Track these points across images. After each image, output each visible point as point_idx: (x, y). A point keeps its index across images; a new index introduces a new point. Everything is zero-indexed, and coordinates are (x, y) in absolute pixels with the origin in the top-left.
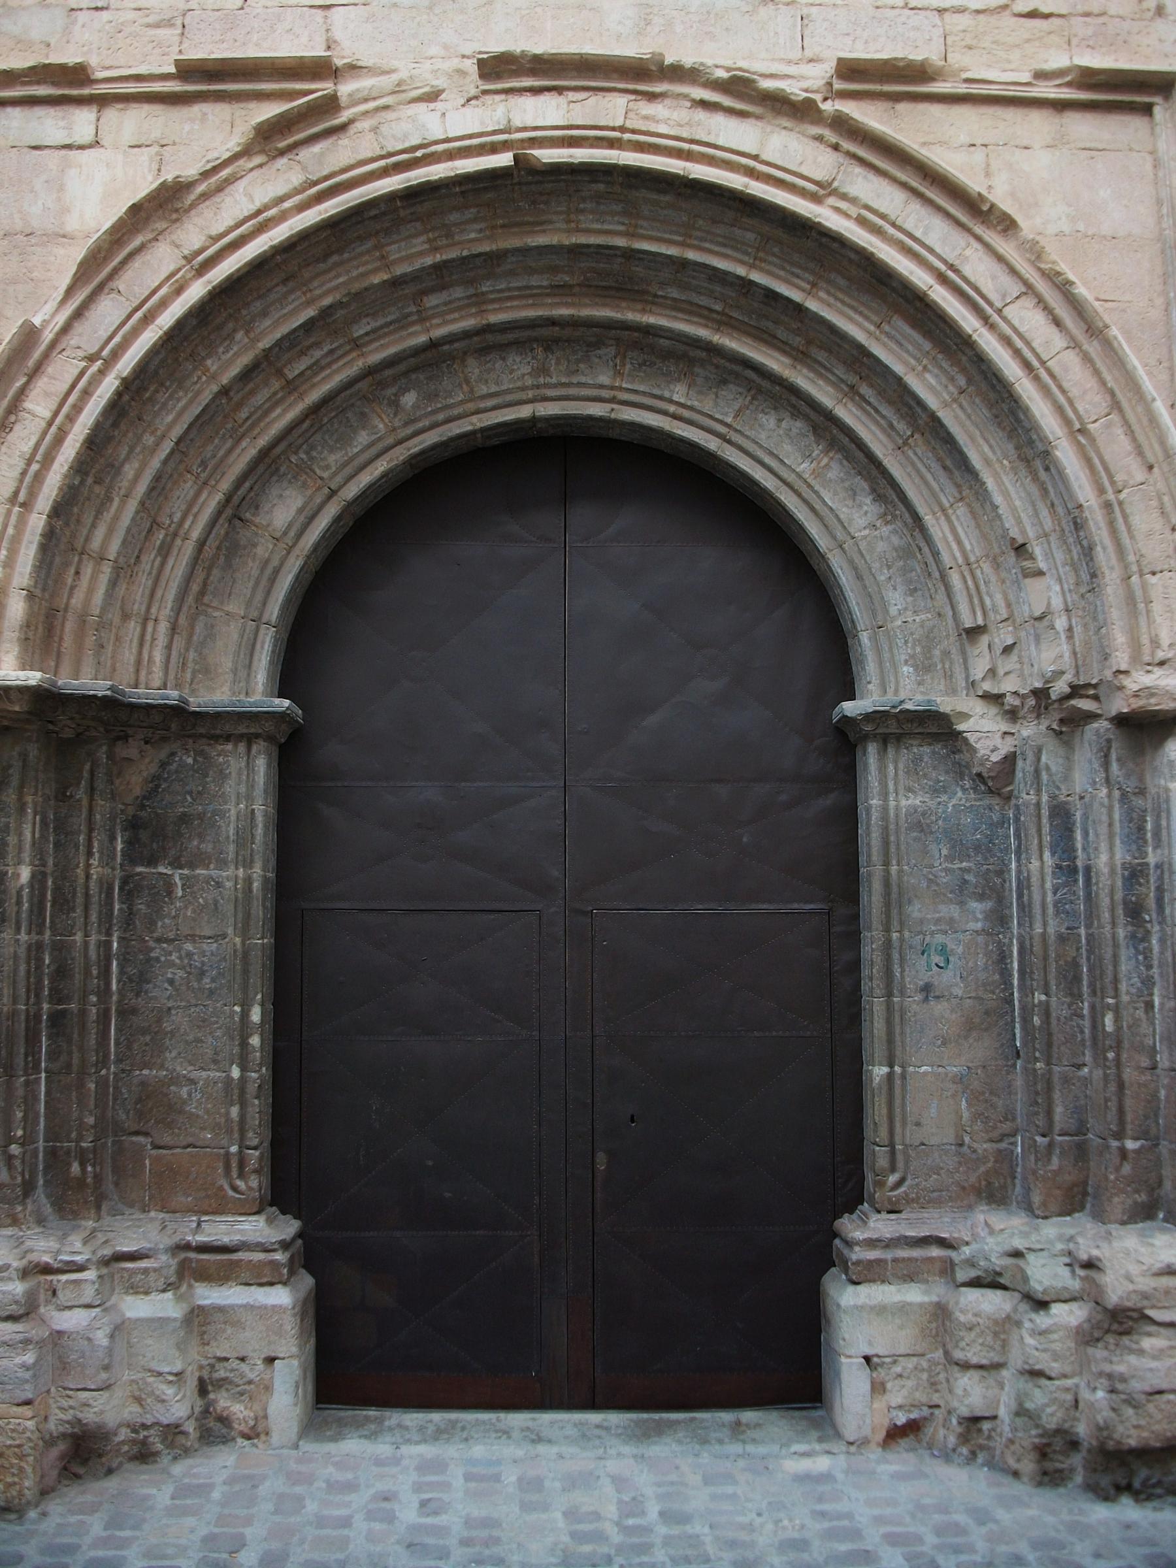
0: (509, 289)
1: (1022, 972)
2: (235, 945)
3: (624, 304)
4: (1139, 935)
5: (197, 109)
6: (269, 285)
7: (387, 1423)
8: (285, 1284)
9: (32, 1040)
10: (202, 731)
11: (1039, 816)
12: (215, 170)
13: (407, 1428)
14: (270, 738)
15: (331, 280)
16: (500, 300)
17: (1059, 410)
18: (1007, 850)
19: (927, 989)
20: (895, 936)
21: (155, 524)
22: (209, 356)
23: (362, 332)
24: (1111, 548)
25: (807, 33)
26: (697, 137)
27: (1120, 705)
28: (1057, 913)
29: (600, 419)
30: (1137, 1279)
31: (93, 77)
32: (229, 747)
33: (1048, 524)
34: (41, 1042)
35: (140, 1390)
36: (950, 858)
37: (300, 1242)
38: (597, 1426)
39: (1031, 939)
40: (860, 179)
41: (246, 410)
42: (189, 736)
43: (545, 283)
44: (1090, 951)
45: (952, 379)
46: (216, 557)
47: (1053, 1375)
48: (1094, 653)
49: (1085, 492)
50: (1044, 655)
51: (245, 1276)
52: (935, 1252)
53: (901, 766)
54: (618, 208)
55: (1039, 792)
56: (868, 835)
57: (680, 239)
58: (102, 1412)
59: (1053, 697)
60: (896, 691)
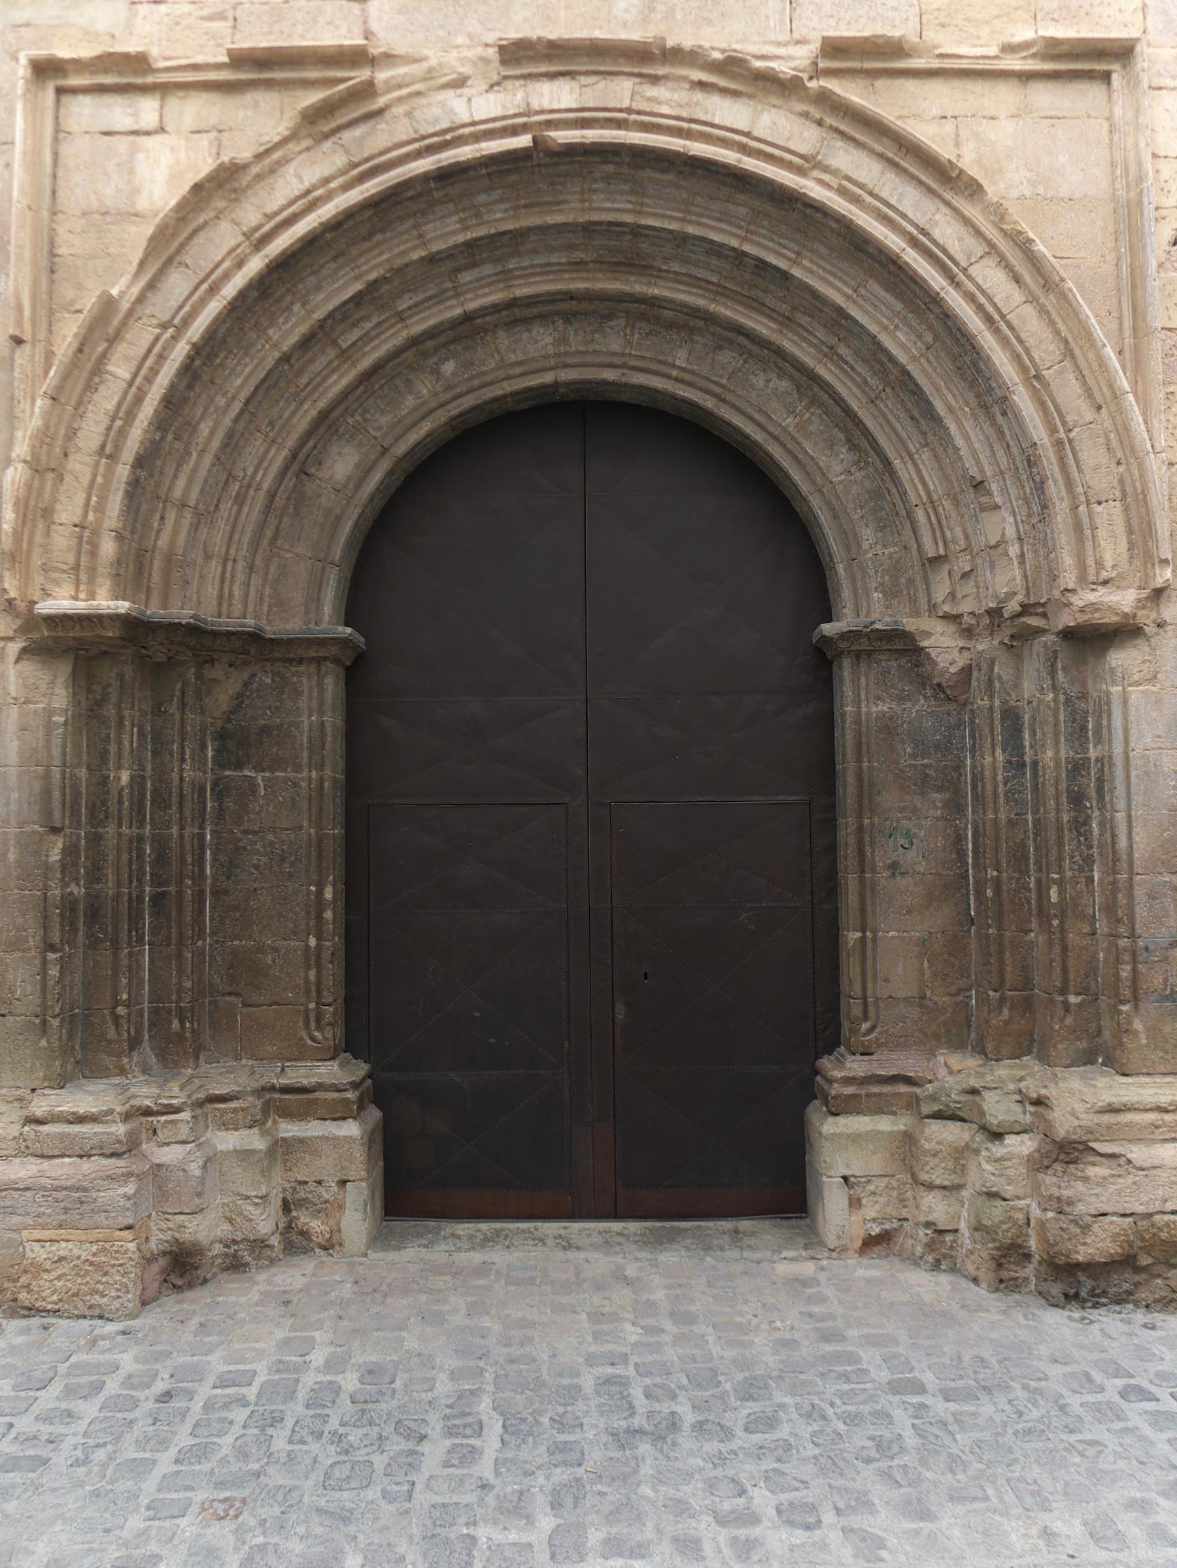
0: (532, 266)
1: (976, 852)
2: (310, 835)
3: (632, 279)
4: (1081, 820)
5: (249, 97)
6: (322, 261)
7: (443, 1233)
8: (355, 1118)
9: (135, 917)
10: (278, 655)
11: (992, 719)
12: (267, 152)
13: (459, 1237)
14: (336, 661)
15: (375, 257)
16: (525, 276)
17: (1017, 358)
18: (963, 749)
19: (894, 866)
20: (866, 822)
21: (231, 476)
22: (270, 325)
23: (405, 306)
24: (1061, 482)
25: (795, 16)
26: (696, 117)
27: (1066, 620)
28: (1007, 801)
29: (614, 383)
30: (1081, 1116)
31: (154, 66)
32: (302, 668)
33: (1004, 463)
34: (144, 919)
35: (231, 1211)
36: (913, 756)
37: (369, 1081)
38: (618, 1234)
39: (984, 823)
40: (841, 152)
41: (306, 375)
42: (267, 660)
43: (564, 260)
44: (1036, 834)
45: (920, 337)
46: (286, 506)
47: (1008, 1197)
48: (1043, 576)
49: (1038, 432)
50: (998, 579)
51: (321, 1112)
52: (903, 1089)
53: (872, 678)
54: (625, 187)
55: (991, 697)
56: (843, 736)
57: (680, 215)
58: (196, 1232)
59: (1006, 616)
60: (868, 615)
